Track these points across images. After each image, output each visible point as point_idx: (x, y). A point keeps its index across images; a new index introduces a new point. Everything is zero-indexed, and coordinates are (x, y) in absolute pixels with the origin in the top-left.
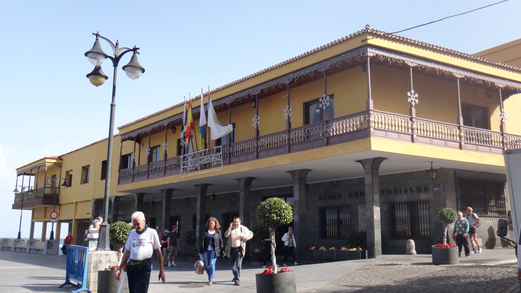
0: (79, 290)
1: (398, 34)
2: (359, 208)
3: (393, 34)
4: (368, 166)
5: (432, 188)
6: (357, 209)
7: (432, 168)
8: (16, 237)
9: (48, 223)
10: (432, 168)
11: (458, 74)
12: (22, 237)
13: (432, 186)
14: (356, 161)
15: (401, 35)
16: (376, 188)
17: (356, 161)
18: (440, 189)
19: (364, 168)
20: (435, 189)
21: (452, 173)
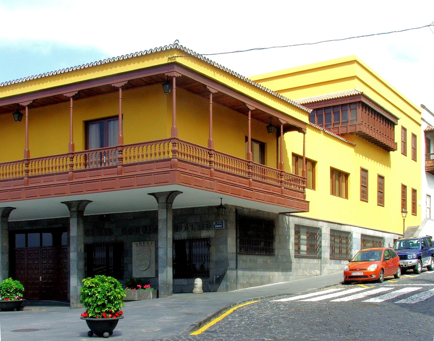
0: (256, 287)
1: (207, 57)
2: (134, 245)
3: (203, 56)
4: (163, 200)
5: (214, 226)
6: (131, 247)
7: (221, 204)
8: (38, 245)
9: (17, 236)
10: (221, 204)
11: (251, 106)
12: (44, 245)
13: (215, 223)
14: (62, 203)
15: (210, 58)
16: (170, 224)
17: (62, 203)
18: (223, 227)
19: (158, 202)
20: (218, 226)
21: (234, 210)
